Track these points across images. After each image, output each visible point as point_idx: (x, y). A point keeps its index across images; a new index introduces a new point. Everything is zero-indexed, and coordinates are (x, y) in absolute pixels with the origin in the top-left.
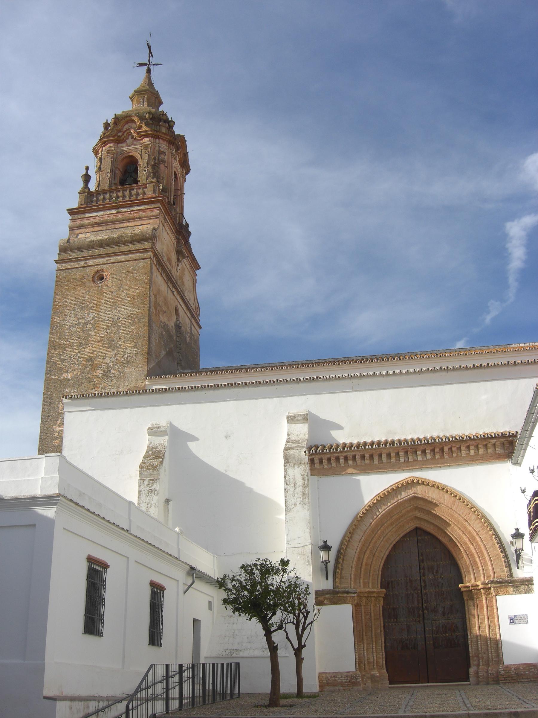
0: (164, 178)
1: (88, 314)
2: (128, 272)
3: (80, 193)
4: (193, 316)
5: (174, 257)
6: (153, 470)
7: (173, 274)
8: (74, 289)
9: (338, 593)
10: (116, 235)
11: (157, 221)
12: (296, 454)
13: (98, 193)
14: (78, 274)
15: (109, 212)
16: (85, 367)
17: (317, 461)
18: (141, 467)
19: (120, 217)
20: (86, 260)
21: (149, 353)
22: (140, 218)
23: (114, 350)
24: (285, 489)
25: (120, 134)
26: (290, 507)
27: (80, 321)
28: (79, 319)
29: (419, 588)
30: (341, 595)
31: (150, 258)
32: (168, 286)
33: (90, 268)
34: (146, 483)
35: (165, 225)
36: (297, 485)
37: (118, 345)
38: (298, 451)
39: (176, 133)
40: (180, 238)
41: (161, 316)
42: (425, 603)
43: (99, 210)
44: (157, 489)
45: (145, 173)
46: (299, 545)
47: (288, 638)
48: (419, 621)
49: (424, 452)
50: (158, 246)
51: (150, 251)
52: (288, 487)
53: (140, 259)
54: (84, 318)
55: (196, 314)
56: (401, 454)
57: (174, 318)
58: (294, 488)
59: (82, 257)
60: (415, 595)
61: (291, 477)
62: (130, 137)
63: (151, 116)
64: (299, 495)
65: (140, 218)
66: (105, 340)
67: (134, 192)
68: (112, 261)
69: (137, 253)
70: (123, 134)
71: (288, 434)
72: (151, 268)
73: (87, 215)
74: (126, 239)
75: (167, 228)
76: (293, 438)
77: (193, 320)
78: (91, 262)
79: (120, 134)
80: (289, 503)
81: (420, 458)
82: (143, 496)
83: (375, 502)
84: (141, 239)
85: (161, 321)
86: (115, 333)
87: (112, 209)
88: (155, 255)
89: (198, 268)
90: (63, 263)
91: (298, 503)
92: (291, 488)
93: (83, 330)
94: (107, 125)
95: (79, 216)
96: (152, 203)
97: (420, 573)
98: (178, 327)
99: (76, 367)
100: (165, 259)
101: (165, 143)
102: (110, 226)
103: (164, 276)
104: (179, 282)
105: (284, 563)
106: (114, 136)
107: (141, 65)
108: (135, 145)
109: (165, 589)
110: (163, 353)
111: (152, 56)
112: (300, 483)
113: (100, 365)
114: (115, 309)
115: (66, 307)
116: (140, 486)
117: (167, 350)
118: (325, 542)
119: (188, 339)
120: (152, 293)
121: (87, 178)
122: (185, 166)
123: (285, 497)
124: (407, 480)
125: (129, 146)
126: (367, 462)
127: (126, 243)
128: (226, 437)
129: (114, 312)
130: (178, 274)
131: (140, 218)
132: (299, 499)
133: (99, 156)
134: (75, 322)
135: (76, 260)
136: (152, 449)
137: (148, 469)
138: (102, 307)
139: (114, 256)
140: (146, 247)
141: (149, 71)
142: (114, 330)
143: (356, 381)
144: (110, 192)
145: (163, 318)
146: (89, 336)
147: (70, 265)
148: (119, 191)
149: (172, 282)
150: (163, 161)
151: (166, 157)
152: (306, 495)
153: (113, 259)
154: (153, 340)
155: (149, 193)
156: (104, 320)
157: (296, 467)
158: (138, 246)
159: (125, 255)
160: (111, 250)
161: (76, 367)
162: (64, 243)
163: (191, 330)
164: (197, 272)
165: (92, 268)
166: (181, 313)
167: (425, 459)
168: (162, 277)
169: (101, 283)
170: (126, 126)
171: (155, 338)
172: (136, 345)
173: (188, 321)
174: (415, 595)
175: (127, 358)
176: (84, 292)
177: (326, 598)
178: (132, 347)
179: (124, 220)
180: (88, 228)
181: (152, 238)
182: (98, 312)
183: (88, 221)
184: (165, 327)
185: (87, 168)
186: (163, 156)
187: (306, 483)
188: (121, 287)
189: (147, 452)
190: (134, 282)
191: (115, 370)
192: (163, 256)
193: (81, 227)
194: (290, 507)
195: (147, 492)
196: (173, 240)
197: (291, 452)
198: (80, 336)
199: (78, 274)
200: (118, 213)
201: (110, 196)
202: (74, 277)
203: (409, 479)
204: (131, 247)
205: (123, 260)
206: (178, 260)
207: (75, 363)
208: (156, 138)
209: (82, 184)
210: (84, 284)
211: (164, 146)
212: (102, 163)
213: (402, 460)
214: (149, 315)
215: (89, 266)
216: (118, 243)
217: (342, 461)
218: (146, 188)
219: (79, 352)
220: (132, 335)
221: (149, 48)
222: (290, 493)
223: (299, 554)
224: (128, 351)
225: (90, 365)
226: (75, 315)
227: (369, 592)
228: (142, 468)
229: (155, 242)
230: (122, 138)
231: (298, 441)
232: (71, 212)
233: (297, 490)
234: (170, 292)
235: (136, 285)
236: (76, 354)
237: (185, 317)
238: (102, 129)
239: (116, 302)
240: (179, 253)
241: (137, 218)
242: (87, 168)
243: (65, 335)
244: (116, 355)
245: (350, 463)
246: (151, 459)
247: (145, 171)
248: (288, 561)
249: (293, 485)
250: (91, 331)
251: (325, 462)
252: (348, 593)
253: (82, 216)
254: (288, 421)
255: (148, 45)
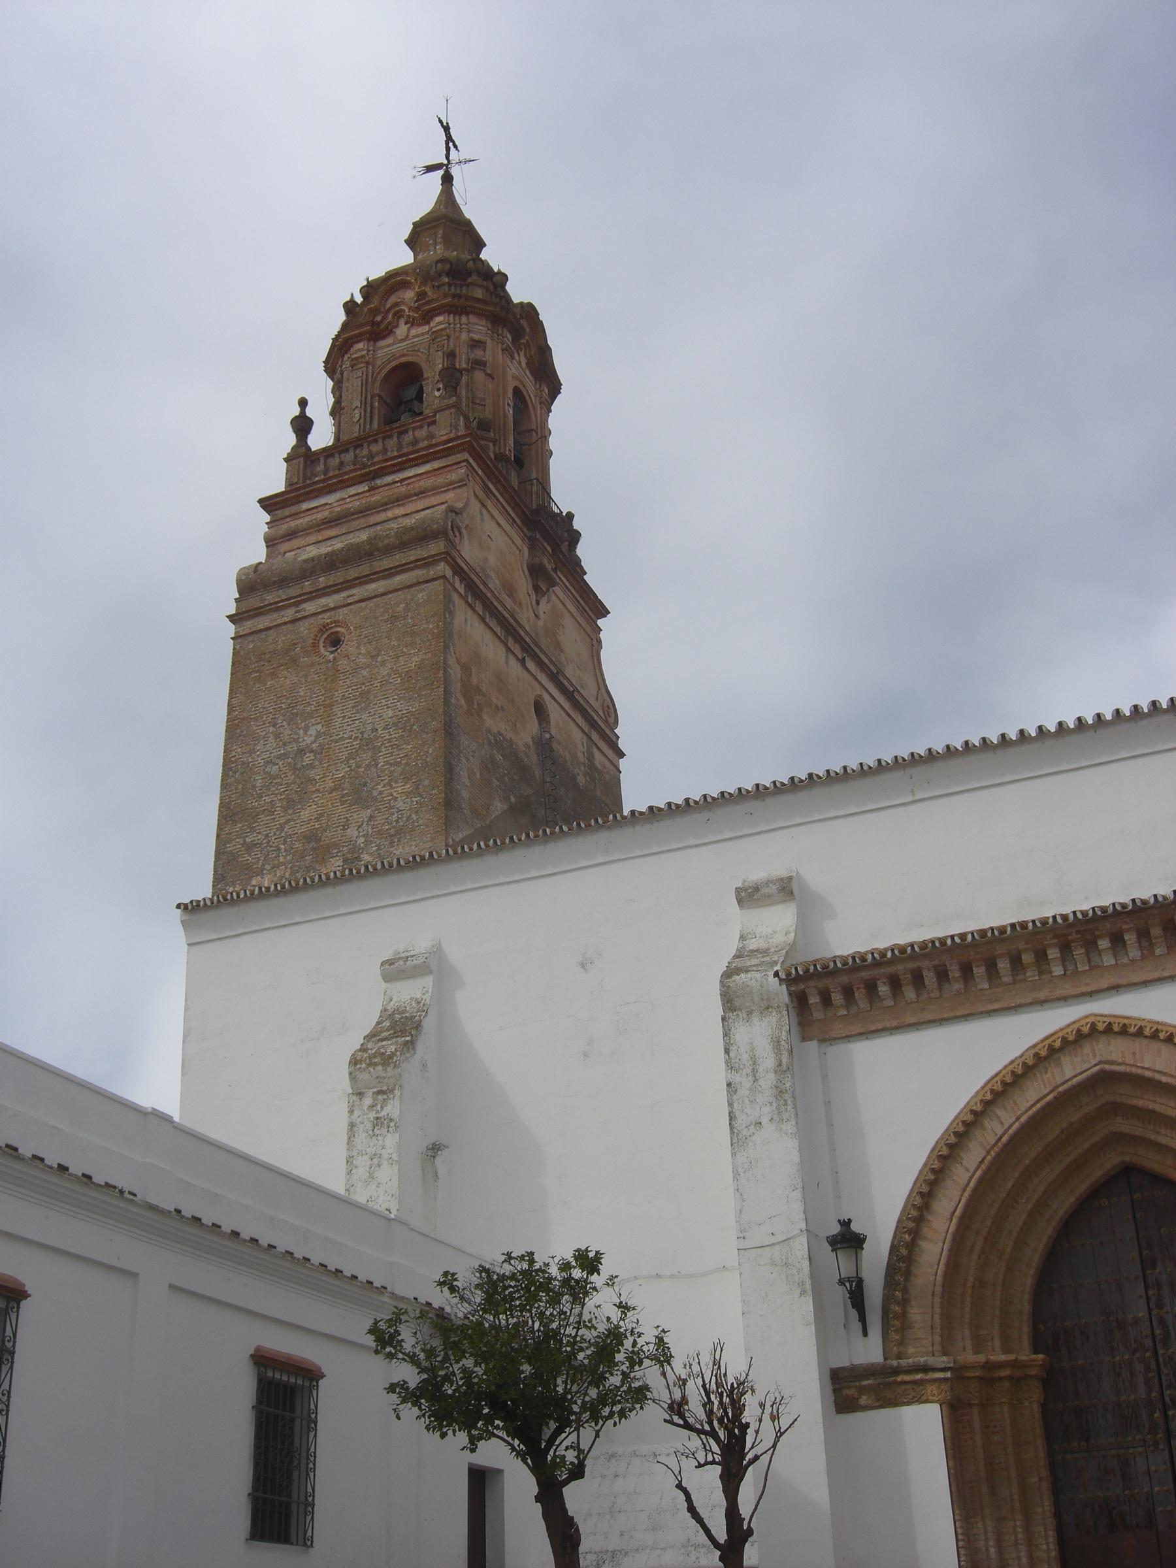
0: (484, 400)
1: (306, 729)
2: (394, 618)
3: (286, 460)
4: (593, 724)
5: (523, 584)
6: (383, 1065)
7: (524, 622)
8: (274, 675)
9: (897, 1371)
10: (363, 536)
11: (463, 492)
12: (753, 983)
13: (327, 452)
14: (280, 640)
15: (353, 490)
16: (302, 857)
17: (814, 999)
18: (354, 1061)
19: (377, 497)
20: (297, 604)
21: (450, 803)
22: (422, 493)
23: (367, 807)
24: (729, 1085)
25: (379, 318)
26: (744, 1132)
27: (288, 748)
28: (285, 744)
29: (1148, 1343)
30: (907, 1378)
31: (444, 577)
32: (508, 649)
33: (306, 622)
34: (368, 1101)
35: (489, 503)
36: (761, 1069)
37: (375, 793)
38: (758, 975)
39: (516, 300)
40: (538, 536)
41: (485, 717)
42: (1169, 1387)
43: (330, 490)
44: (395, 1114)
45: (437, 394)
46: (774, 1240)
47: (692, 1509)
48: (1156, 1444)
49: (1117, 940)
50: (469, 552)
51: (440, 560)
52: (736, 1078)
53: (418, 583)
54: (296, 740)
55: (606, 722)
56: (1053, 953)
57: (533, 726)
58: (751, 1078)
59: (287, 599)
60: (1139, 1367)
61: (742, 1050)
62: (402, 321)
63: (448, 266)
64: (766, 1094)
65: (421, 493)
66: (347, 785)
67: (408, 438)
68: (356, 598)
69: (411, 569)
70: (384, 318)
71: (742, 938)
72: (448, 601)
73: (305, 506)
74: (386, 541)
75: (496, 514)
76: (753, 945)
77: (595, 736)
78: (310, 607)
79: (379, 318)
80: (741, 1122)
81: (1108, 960)
82: (361, 1139)
83: (989, 1097)
84: (424, 535)
85: (489, 731)
86: (368, 766)
87: (360, 483)
88: (458, 570)
89: (603, 612)
90: (245, 619)
91: (765, 1120)
92: (743, 1080)
93: (294, 768)
94: (350, 307)
95: (286, 512)
96: (448, 452)
97: (1148, 1299)
98: (545, 747)
99: (281, 860)
100: (495, 583)
101: (484, 322)
102: (357, 523)
103: (493, 623)
104: (544, 642)
105: (589, 1262)
106: (363, 325)
107: (430, 169)
108: (414, 337)
109: (322, 1376)
110: (499, 806)
111: (455, 146)
112: (768, 1062)
113: (336, 846)
114: (365, 709)
115: (256, 719)
116: (351, 1112)
117: (513, 799)
118: (846, 1224)
119: (581, 779)
120: (452, 661)
121: (302, 425)
122: (549, 382)
123: (730, 1105)
124: (1075, 1026)
125: (402, 340)
126: (958, 986)
127: (388, 550)
128: (583, 965)
129: (365, 716)
130: (541, 623)
131: (422, 493)
132: (766, 1109)
133: (337, 376)
134: (276, 753)
135: (276, 608)
136: (392, 1015)
137: (370, 1064)
138: (337, 709)
139: (360, 584)
140: (433, 553)
141: (447, 179)
142: (366, 757)
143: (919, 771)
144: (356, 447)
145: (494, 724)
146: (310, 780)
147: (263, 622)
148: (376, 441)
149: (519, 639)
150: (479, 364)
151: (489, 352)
152: (786, 1096)
153: (358, 592)
154: (464, 774)
155: (442, 431)
156: (343, 739)
157: (755, 1020)
158: (414, 554)
159: (384, 578)
160: (353, 573)
161: (281, 860)
162: (247, 575)
163: (591, 757)
164: (600, 622)
165: (312, 620)
166: (555, 714)
167: (1125, 960)
168: (487, 625)
169: (332, 652)
170: (393, 299)
171: (468, 769)
172: (417, 788)
173: (578, 736)
174: (1139, 1367)
175: (397, 821)
176: (295, 679)
177: (860, 1387)
178: (408, 794)
179: (386, 504)
180: (308, 534)
181: (446, 531)
182: (328, 722)
183: (307, 519)
184: (500, 743)
185: (303, 403)
186: (478, 353)
187: (784, 1061)
188: (378, 655)
189: (378, 1023)
190: (408, 639)
191: (371, 854)
192: (487, 576)
193: (292, 535)
194: (744, 1132)
195: (369, 1126)
196: (519, 541)
197: (742, 978)
198: (288, 785)
199: (280, 640)
200: (371, 489)
201: (356, 456)
202: (271, 648)
203: (1083, 1022)
204: (399, 558)
205: (381, 590)
206: (536, 588)
207: (279, 849)
208: (461, 314)
209: (291, 439)
210: (294, 661)
211: (479, 328)
212: (344, 390)
213: (1058, 970)
214: (447, 714)
215: (306, 617)
216: (370, 554)
217: (883, 989)
218: (434, 422)
219: (288, 821)
220: (407, 764)
221: (447, 129)
222: (743, 1092)
223: (773, 1264)
224: (400, 804)
225: (314, 849)
226: (277, 736)
227: (988, 1366)
228: (356, 1064)
229: (457, 540)
230: (382, 326)
231: (765, 952)
232: (267, 504)
233: (761, 1082)
234: (513, 662)
235: (412, 645)
236: (282, 827)
237: (564, 726)
238: (342, 317)
239: (369, 692)
240: (536, 571)
241: (416, 495)
242: (303, 403)
243: (254, 787)
244: (371, 818)
245: (910, 993)
246: (382, 1040)
247: (439, 390)
248: (598, 1256)
249: (749, 1070)
250: (314, 767)
251: (837, 998)
252: (925, 1369)
253: (294, 509)
254: (740, 901)
255: (441, 122)
